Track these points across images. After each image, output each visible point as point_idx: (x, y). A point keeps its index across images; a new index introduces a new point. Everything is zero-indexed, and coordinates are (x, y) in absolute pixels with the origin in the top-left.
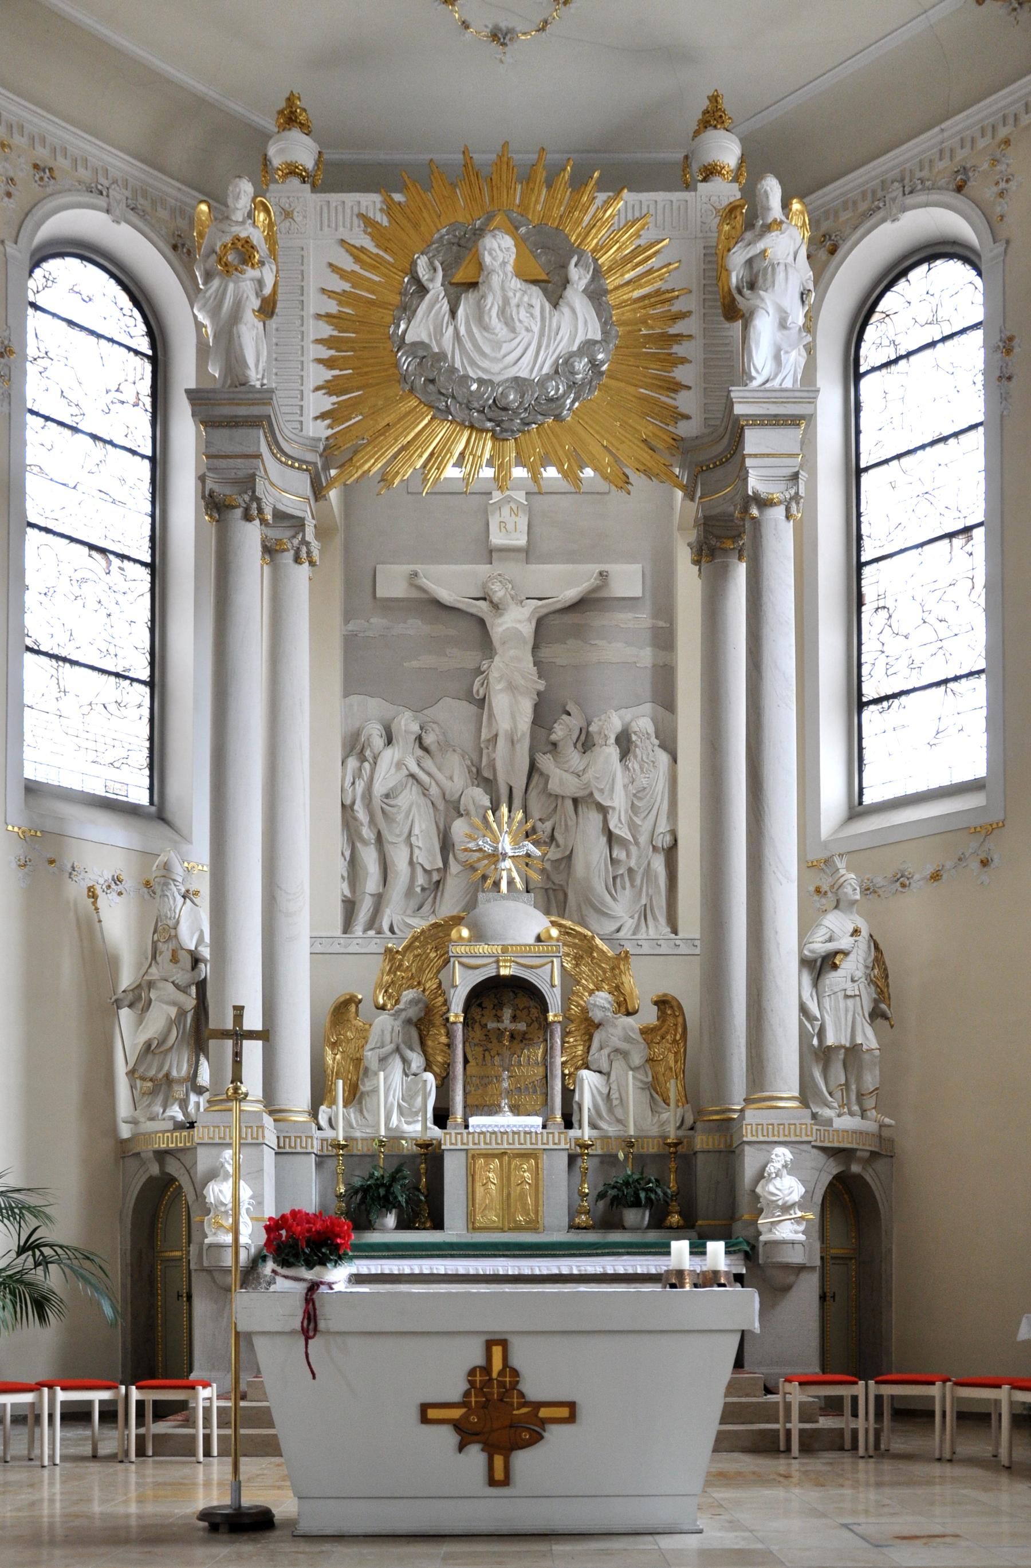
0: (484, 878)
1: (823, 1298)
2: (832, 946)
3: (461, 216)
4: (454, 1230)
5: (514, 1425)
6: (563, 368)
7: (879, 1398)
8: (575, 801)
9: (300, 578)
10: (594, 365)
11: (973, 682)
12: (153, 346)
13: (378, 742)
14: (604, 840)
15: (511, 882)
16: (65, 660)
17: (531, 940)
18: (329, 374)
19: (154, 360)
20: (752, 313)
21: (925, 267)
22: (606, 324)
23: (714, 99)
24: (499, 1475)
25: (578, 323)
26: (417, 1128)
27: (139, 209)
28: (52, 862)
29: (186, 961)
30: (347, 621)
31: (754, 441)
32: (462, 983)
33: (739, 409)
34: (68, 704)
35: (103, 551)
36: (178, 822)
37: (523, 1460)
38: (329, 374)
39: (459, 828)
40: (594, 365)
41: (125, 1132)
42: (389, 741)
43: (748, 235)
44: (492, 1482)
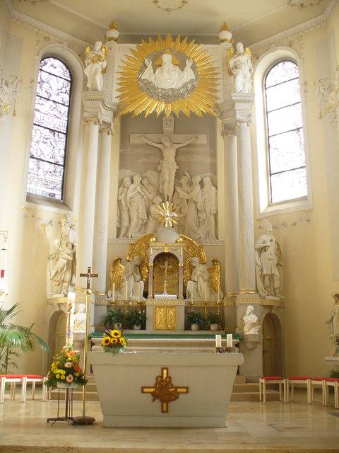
0: (160, 223)
1: (264, 352)
2: (265, 245)
3: (158, 50)
4: (148, 331)
5: (170, 394)
6: (185, 85)
7: (290, 384)
8: (187, 200)
9: (108, 139)
10: (193, 86)
11: (302, 170)
12: (71, 78)
13: (129, 183)
14: (196, 211)
15: (168, 223)
16: (41, 160)
17: (174, 241)
18: (119, 87)
19: (71, 82)
20: (236, 75)
21: (282, 63)
22: (197, 75)
23: (225, 24)
24: (165, 409)
25: (189, 75)
26: (139, 298)
27: (71, 46)
28: (33, 216)
29: (70, 246)
30: (121, 149)
31: (238, 106)
32: (153, 254)
33: (233, 98)
34: (40, 172)
35: (53, 131)
36: (69, 205)
37: (172, 404)
38: (119, 87)
39: (153, 208)
40: (193, 86)
41: (49, 297)
42: (132, 182)
43: (235, 56)
44: (163, 411)
